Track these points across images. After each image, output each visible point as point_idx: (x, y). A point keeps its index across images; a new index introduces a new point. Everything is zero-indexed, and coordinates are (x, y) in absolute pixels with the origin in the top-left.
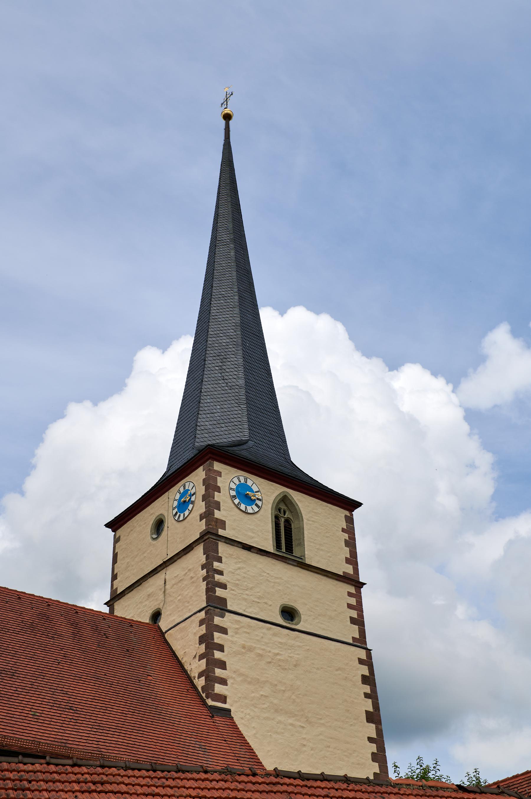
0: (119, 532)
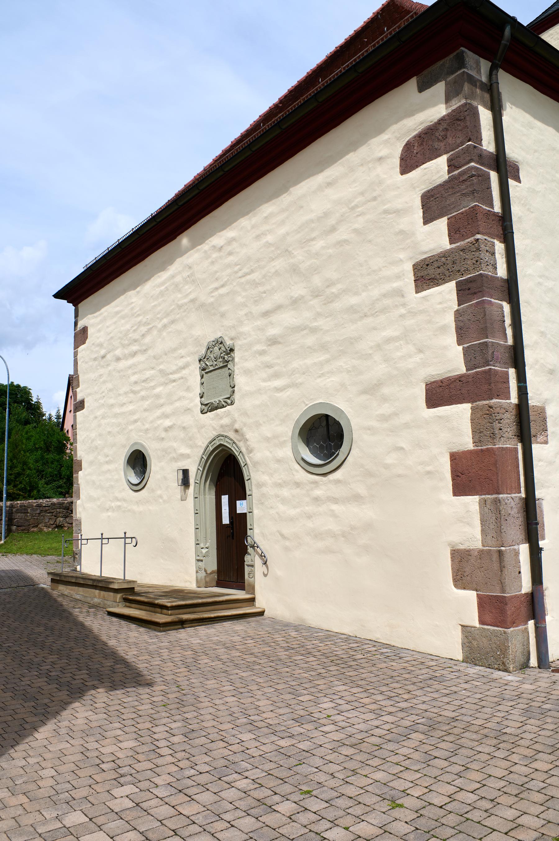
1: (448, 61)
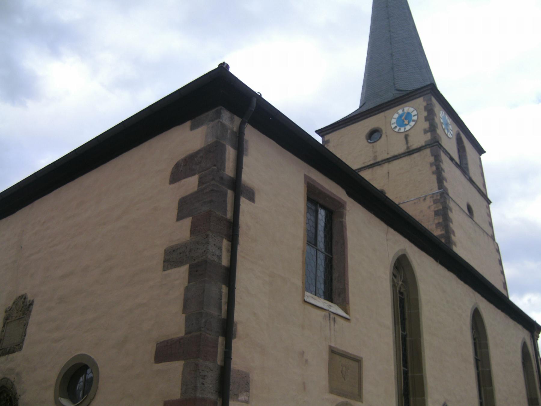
0: (327, 137)
1: (211, 113)
